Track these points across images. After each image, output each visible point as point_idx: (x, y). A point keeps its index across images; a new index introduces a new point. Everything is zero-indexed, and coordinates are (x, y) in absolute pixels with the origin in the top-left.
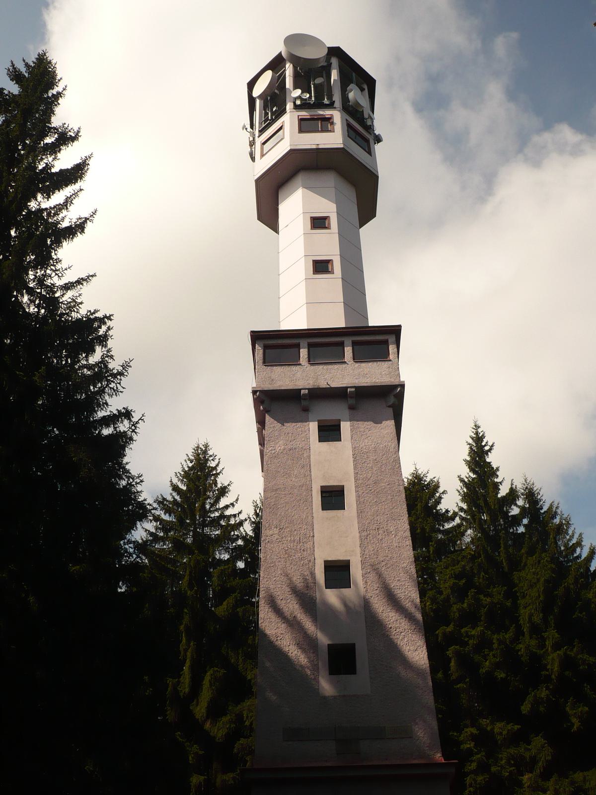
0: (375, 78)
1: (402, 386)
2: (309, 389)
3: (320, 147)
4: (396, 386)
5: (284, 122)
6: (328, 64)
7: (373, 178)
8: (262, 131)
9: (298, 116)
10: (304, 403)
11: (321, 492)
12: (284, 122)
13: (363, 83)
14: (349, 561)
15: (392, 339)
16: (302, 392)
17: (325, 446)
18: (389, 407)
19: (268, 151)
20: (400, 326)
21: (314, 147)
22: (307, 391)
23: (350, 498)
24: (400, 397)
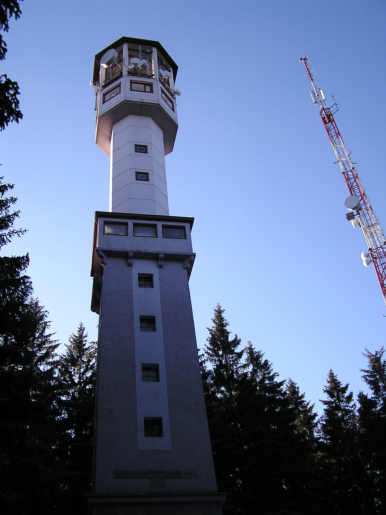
0: (19, 100)
1: (194, 255)
2: (165, 254)
3: (144, 101)
4: (190, 256)
5: (120, 82)
6: (150, 51)
7: (175, 127)
8: (104, 87)
9: (130, 80)
10: (161, 263)
11: (140, 319)
12: (120, 82)
13: (170, 68)
14: (158, 364)
15: (187, 225)
16: (160, 255)
17: (143, 290)
18: (185, 269)
19: (109, 100)
20: (193, 218)
21: (141, 101)
22: (163, 255)
23: (159, 323)
24: (192, 263)
